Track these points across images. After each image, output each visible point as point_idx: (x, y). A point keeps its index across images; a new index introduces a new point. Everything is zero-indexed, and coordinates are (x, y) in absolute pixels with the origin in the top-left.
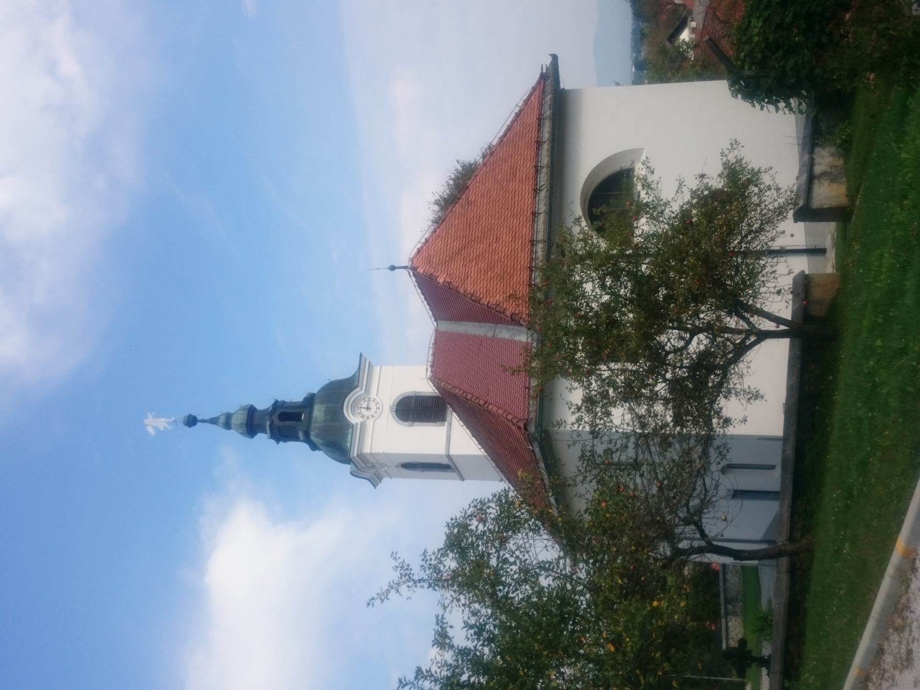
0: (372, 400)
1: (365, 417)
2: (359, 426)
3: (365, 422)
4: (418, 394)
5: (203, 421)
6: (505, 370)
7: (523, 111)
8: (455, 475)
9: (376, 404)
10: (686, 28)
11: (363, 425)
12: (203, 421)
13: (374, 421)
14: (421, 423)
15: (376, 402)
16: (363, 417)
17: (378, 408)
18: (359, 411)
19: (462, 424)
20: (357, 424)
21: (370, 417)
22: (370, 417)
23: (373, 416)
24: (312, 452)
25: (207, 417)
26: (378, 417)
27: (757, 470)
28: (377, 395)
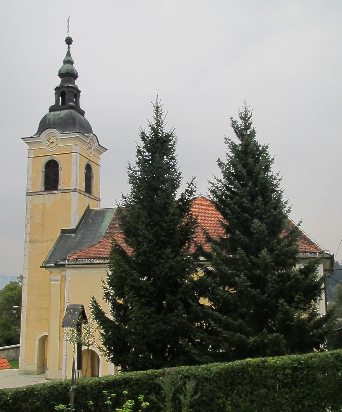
5: (69, 48)
12: (69, 48)
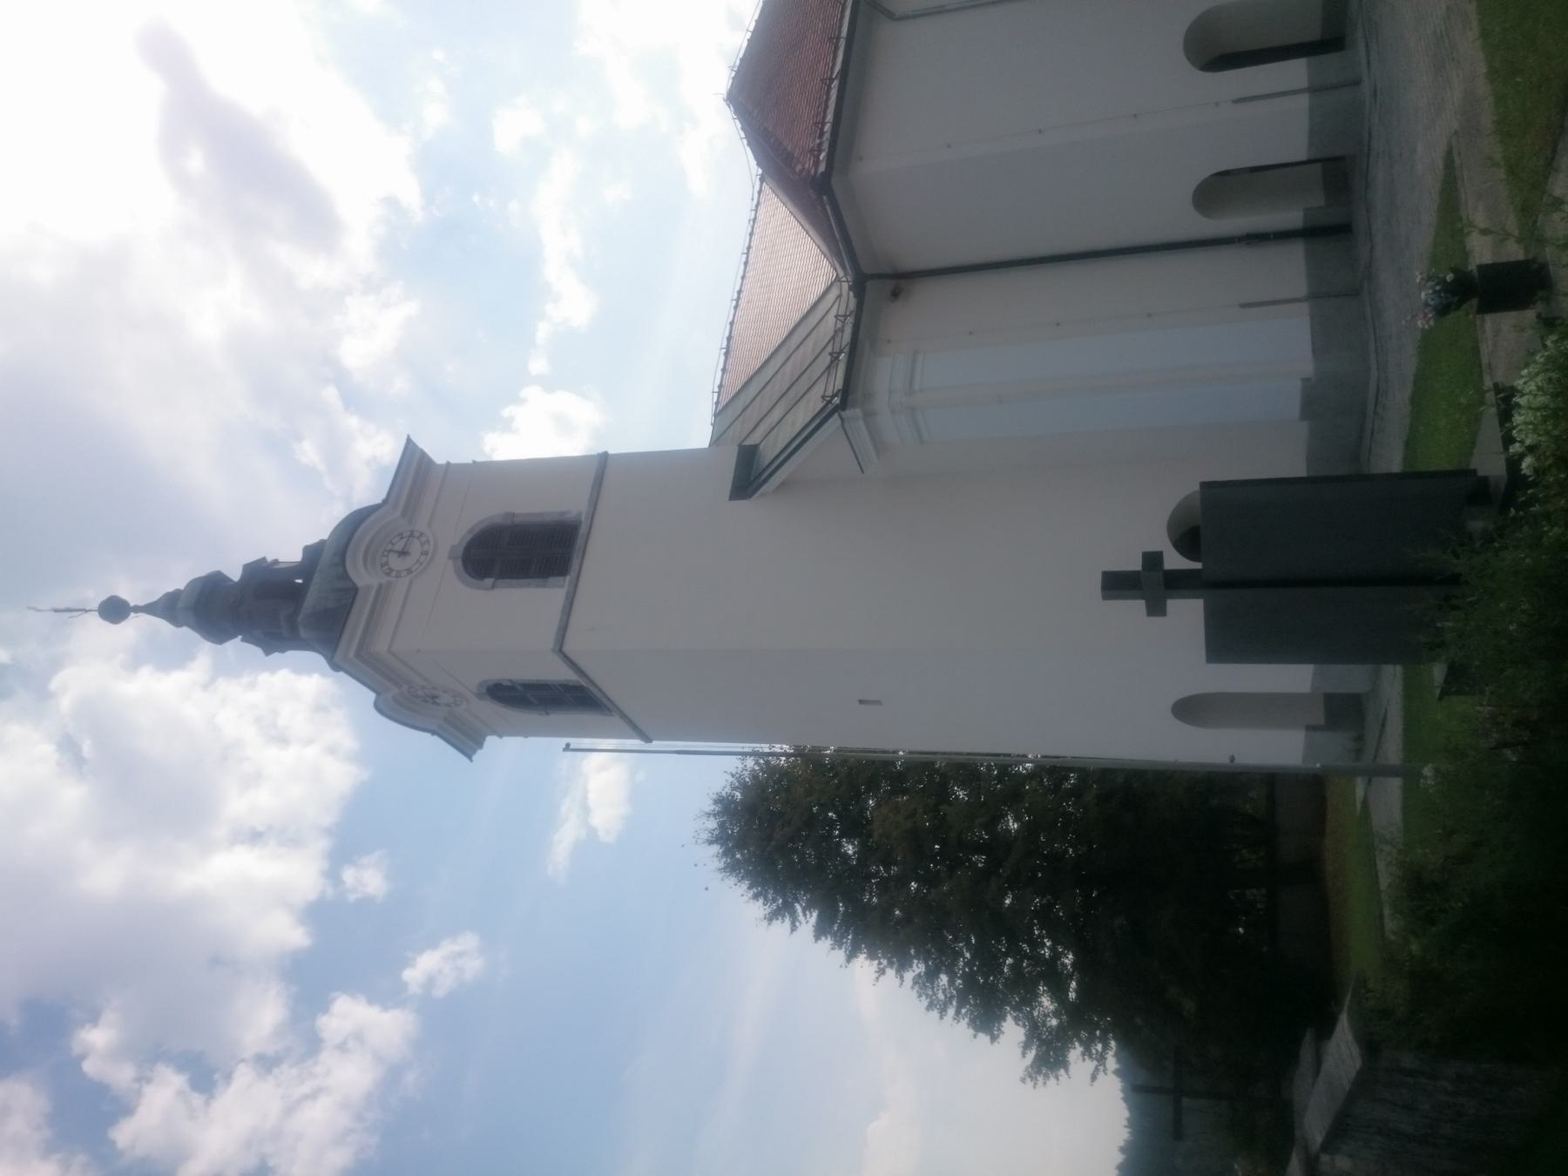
0: (417, 534)
1: (394, 574)
5: (137, 609)
7: (1455, 152)
8: (615, 720)
9: (391, 570)
11: (382, 592)
12: (137, 609)
13: (411, 582)
14: (514, 581)
15: (423, 539)
16: (388, 574)
17: (425, 553)
18: (385, 559)
23: (409, 571)
24: (303, 546)
25: (142, 603)
27: (779, 342)
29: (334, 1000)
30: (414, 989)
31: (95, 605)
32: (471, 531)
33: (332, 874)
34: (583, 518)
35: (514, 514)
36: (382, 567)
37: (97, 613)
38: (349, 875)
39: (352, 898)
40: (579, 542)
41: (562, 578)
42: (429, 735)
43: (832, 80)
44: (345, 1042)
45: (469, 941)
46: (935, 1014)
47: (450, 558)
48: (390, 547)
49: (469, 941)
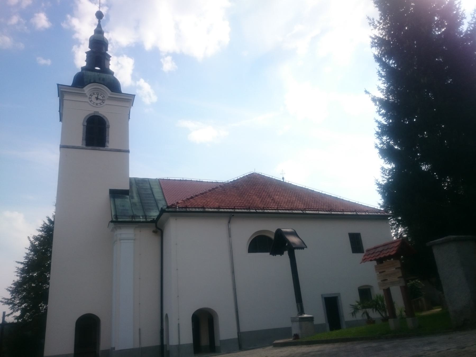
0: (104, 101)
1: (90, 97)
2: (82, 92)
3: (87, 96)
4: (107, 129)
6: (37, 230)
9: (92, 96)
10: (286, 238)
11: (84, 95)
12: (99, 21)
15: (102, 103)
16: (90, 95)
19: (359, 203)
20: (84, 91)
21: (90, 100)
22: (90, 100)
25: (101, 23)
26: (90, 104)
28: (107, 104)
29: (132, 59)
30: (138, 83)
31: (101, 10)
32: (104, 116)
33: (168, 54)
34: (106, 148)
35: (109, 128)
36: (93, 93)
37: (99, 10)
38: (169, 58)
39: (162, 60)
40: (101, 148)
41: (85, 144)
42: (59, 110)
43: (256, 209)
44: (119, 64)
45: (154, 99)
46: (25, 255)
47: (95, 112)
48: (100, 94)
49: (154, 99)
